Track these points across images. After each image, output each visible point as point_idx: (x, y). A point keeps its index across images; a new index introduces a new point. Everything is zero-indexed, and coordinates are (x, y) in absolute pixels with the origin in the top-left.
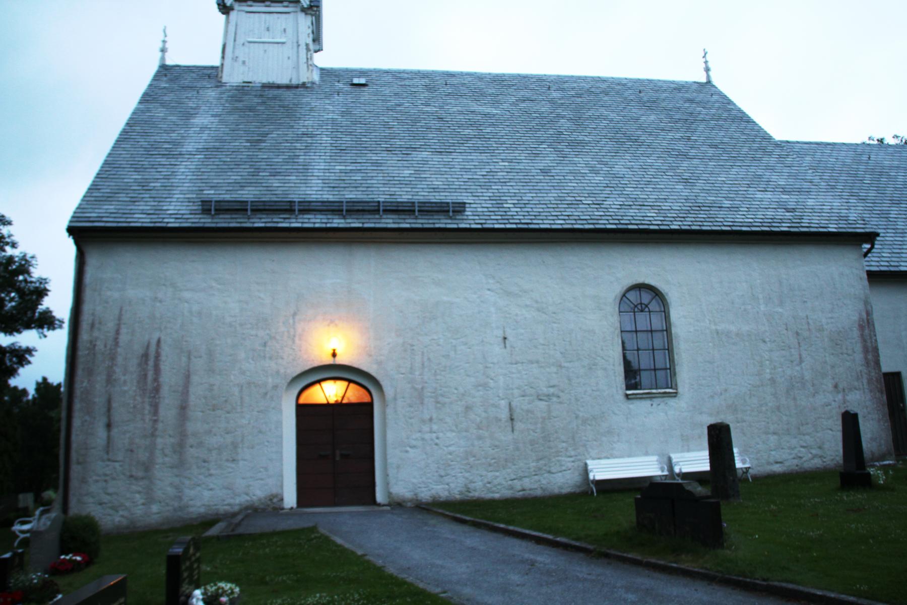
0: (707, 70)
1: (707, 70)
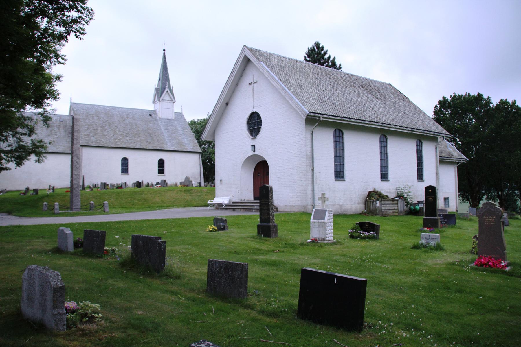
0: (182, 110)
1: (182, 110)
